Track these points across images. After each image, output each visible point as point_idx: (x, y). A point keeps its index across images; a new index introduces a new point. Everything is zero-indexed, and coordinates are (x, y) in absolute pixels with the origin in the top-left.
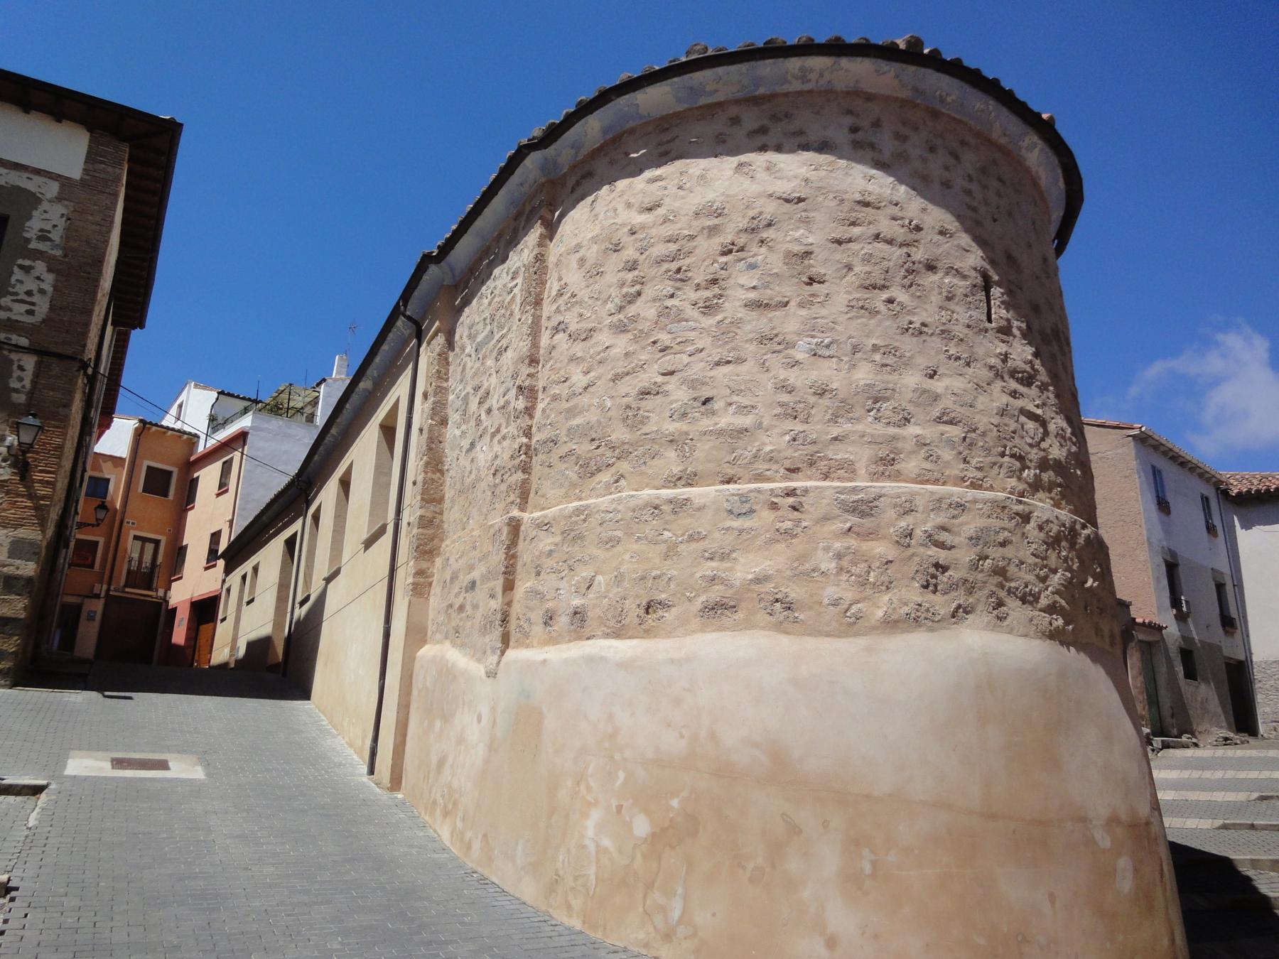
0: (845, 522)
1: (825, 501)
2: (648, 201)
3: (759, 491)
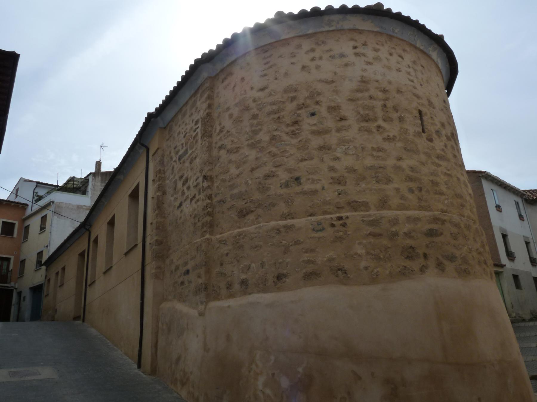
3: (325, 219)
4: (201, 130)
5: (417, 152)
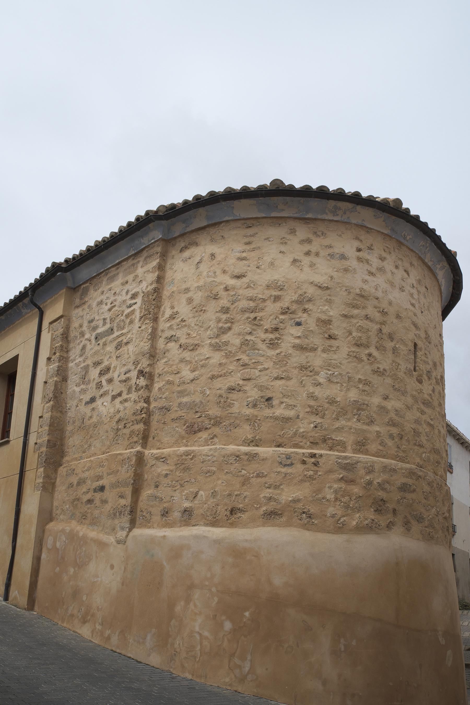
0: (340, 474)
1: (331, 462)
2: (237, 271)
3: (297, 453)
4: (141, 308)
5: (404, 393)
